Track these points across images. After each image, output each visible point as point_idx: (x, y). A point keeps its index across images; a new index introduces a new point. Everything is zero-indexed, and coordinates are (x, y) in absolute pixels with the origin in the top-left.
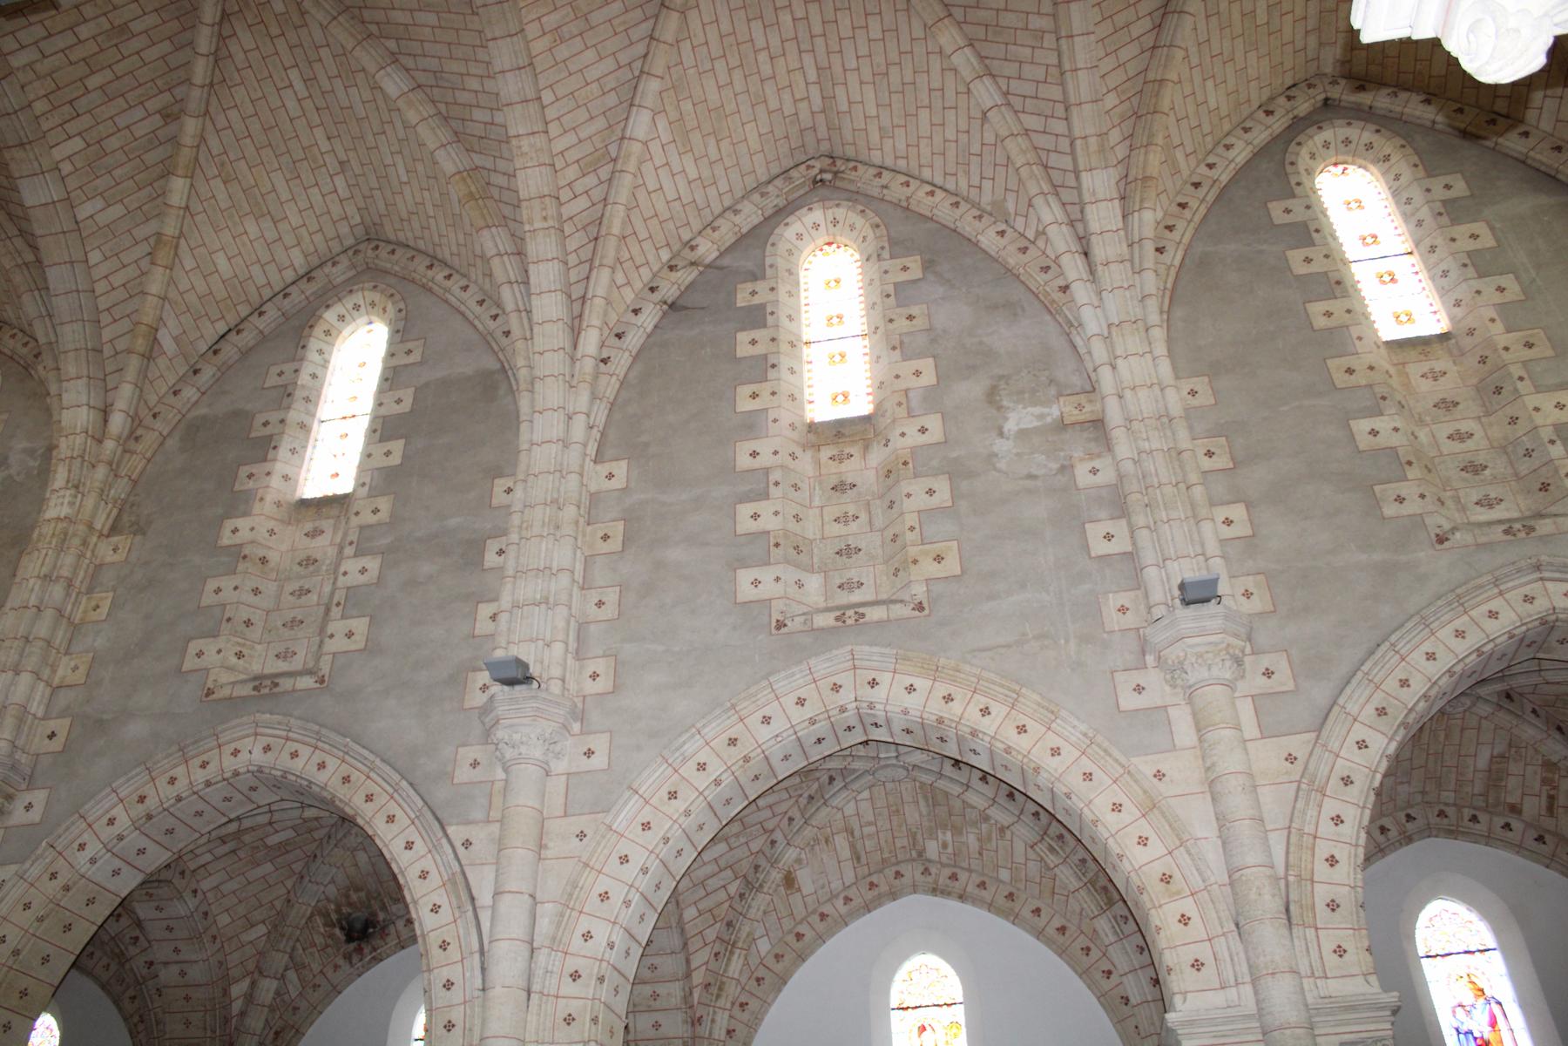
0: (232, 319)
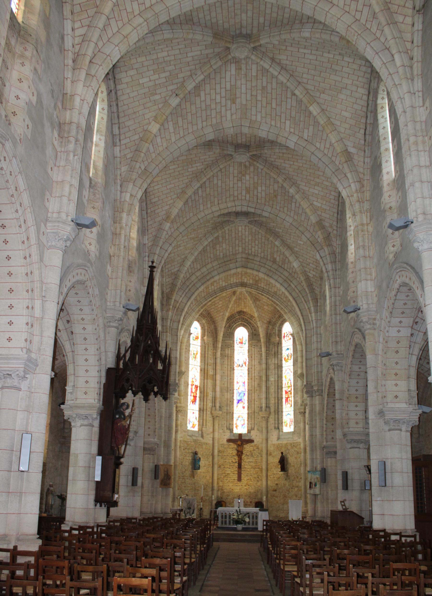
0: (363, 126)
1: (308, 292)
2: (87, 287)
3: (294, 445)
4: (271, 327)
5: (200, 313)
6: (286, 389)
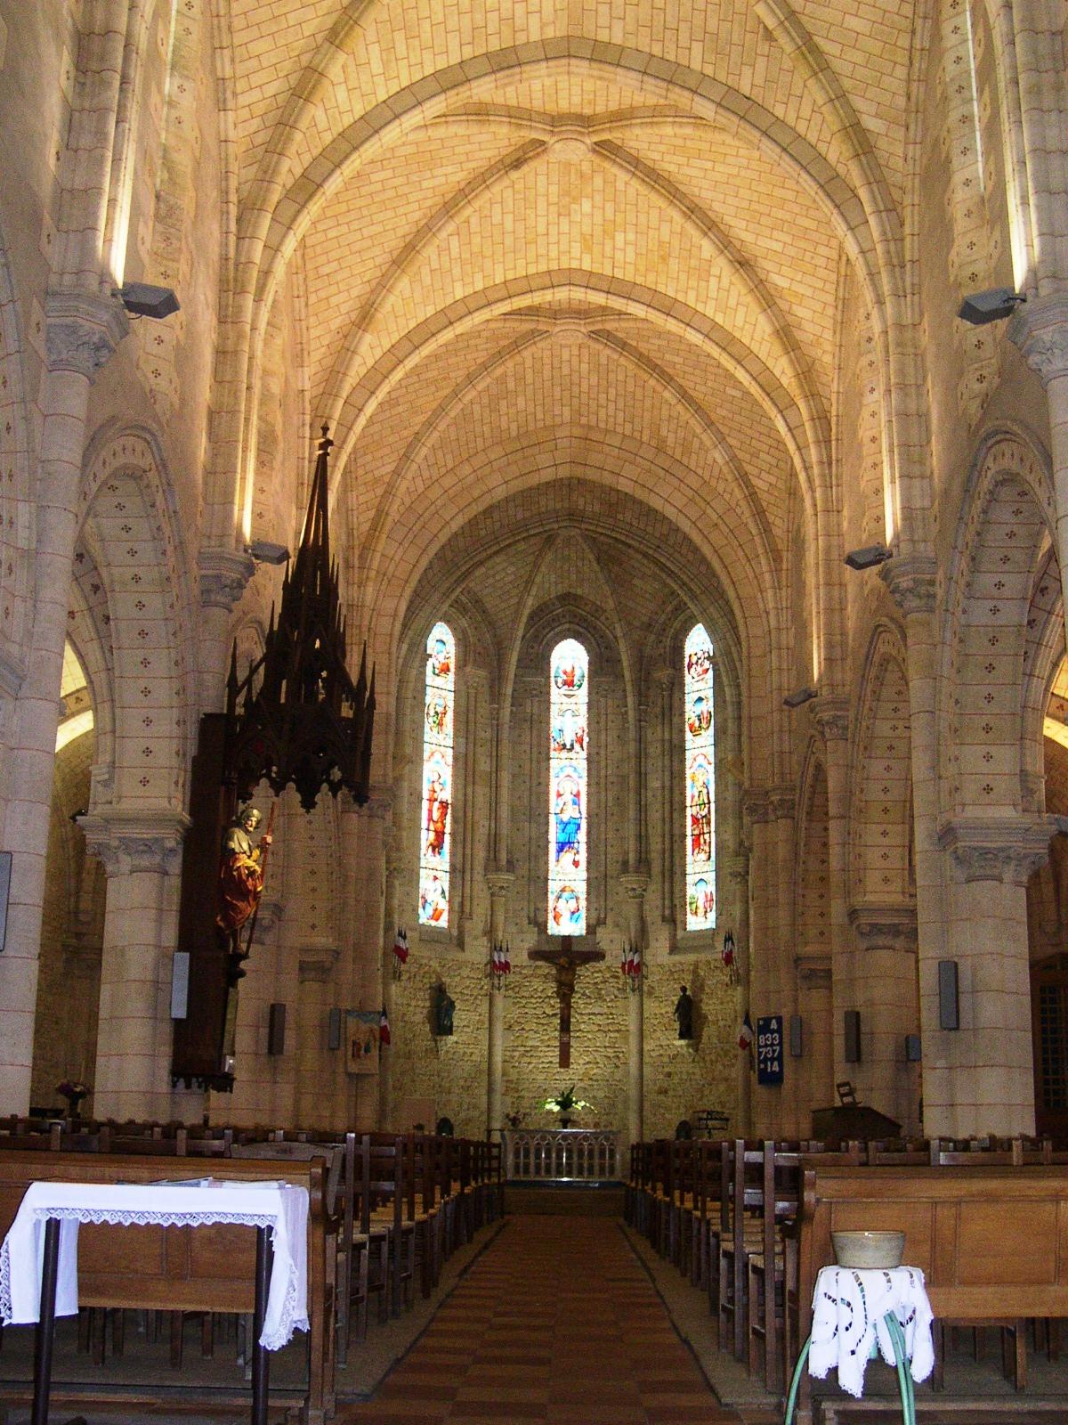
1: (754, 532)
2: (148, 486)
5: (453, 597)
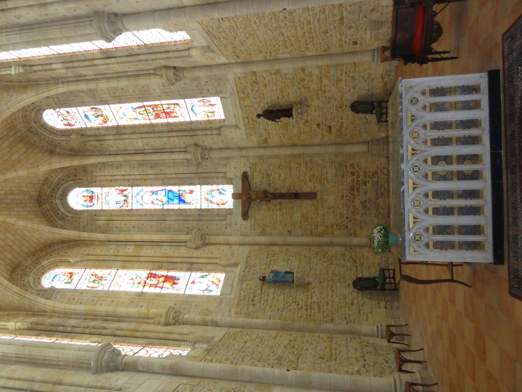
3: (242, 94)
4: (58, 150)
6: (152, 117)
